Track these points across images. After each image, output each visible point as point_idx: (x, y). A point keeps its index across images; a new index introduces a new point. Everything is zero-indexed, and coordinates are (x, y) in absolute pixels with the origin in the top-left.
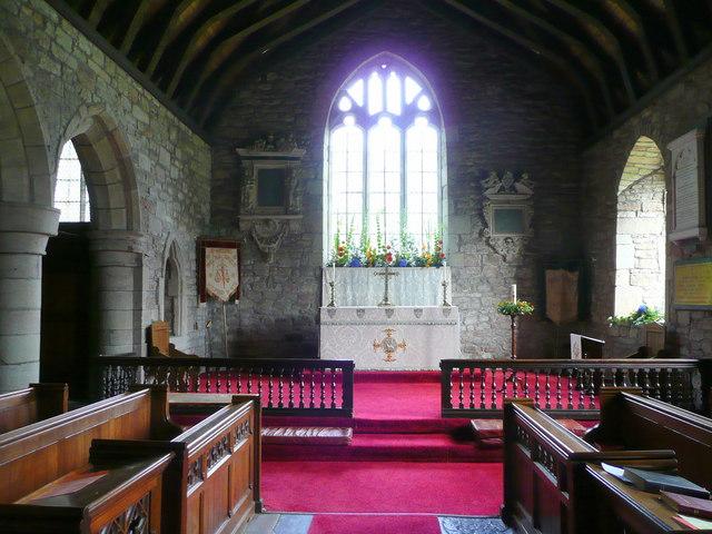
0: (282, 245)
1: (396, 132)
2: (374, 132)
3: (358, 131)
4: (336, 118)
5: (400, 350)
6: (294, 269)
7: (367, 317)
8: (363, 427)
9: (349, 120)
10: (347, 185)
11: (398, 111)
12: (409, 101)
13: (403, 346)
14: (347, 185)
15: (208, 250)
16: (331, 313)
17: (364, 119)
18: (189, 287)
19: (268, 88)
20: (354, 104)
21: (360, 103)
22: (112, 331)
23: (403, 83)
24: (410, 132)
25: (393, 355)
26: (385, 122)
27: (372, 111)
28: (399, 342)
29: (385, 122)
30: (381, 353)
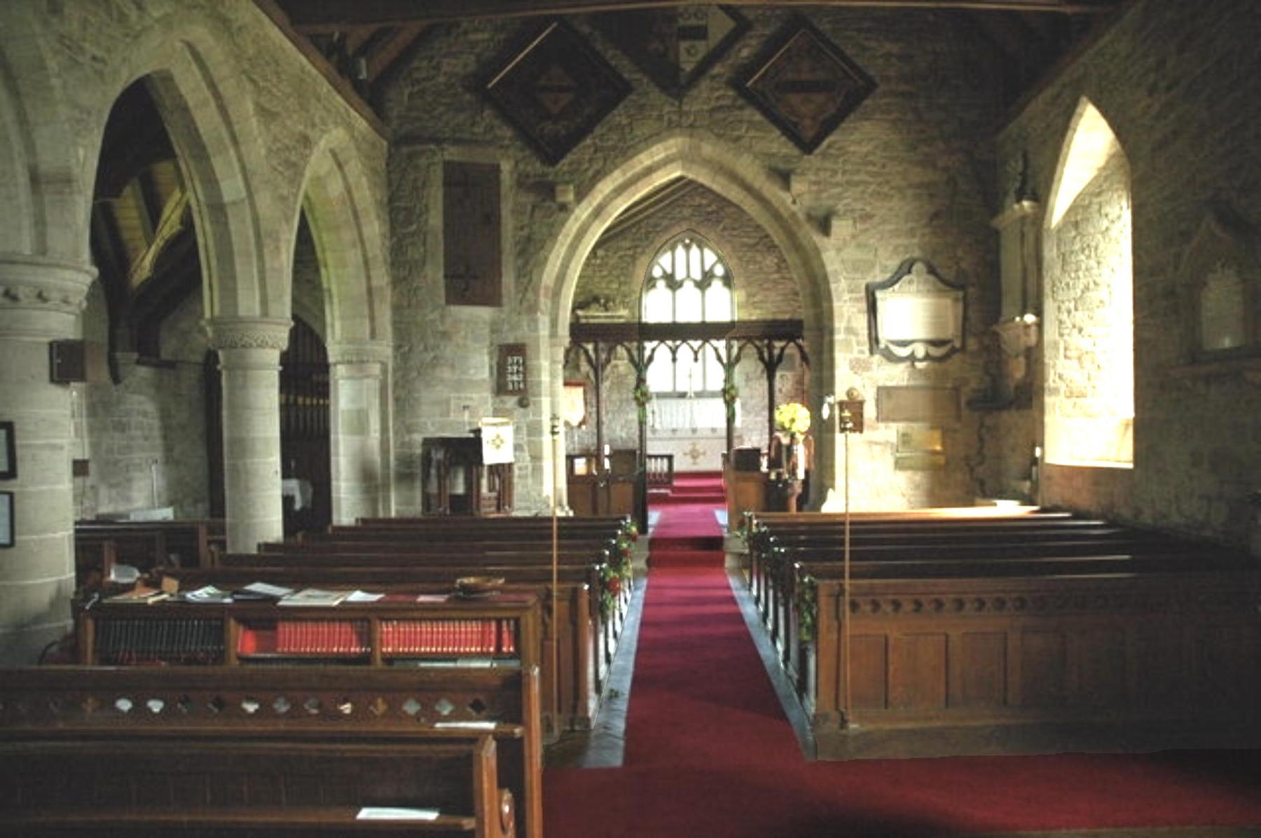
0: (613, 383)
1: (698, 292)
2: (679, 292)
3: (669, 292)
4: (650, 282)
5: (701, 457)
6: (621, 401)
7: (678, 434)
8: (674, 489)
9: (661, 284)
10: (847, 505)
11: (698, 276)
12: (707, 268)
13: (704, 453)
14: (847, 505)
17: (673, 283)
18: (347, 480)
19: (598, 261)
20: (664, 272)
21: (669, 271)
22: (1122, 166)
23: (688, 344)
24: (709, 291)
25: (698, 460)
26: (689, 285)
27: (679, 276)
28: (701, 451)
29: (689, 285)
30: (689, 459)
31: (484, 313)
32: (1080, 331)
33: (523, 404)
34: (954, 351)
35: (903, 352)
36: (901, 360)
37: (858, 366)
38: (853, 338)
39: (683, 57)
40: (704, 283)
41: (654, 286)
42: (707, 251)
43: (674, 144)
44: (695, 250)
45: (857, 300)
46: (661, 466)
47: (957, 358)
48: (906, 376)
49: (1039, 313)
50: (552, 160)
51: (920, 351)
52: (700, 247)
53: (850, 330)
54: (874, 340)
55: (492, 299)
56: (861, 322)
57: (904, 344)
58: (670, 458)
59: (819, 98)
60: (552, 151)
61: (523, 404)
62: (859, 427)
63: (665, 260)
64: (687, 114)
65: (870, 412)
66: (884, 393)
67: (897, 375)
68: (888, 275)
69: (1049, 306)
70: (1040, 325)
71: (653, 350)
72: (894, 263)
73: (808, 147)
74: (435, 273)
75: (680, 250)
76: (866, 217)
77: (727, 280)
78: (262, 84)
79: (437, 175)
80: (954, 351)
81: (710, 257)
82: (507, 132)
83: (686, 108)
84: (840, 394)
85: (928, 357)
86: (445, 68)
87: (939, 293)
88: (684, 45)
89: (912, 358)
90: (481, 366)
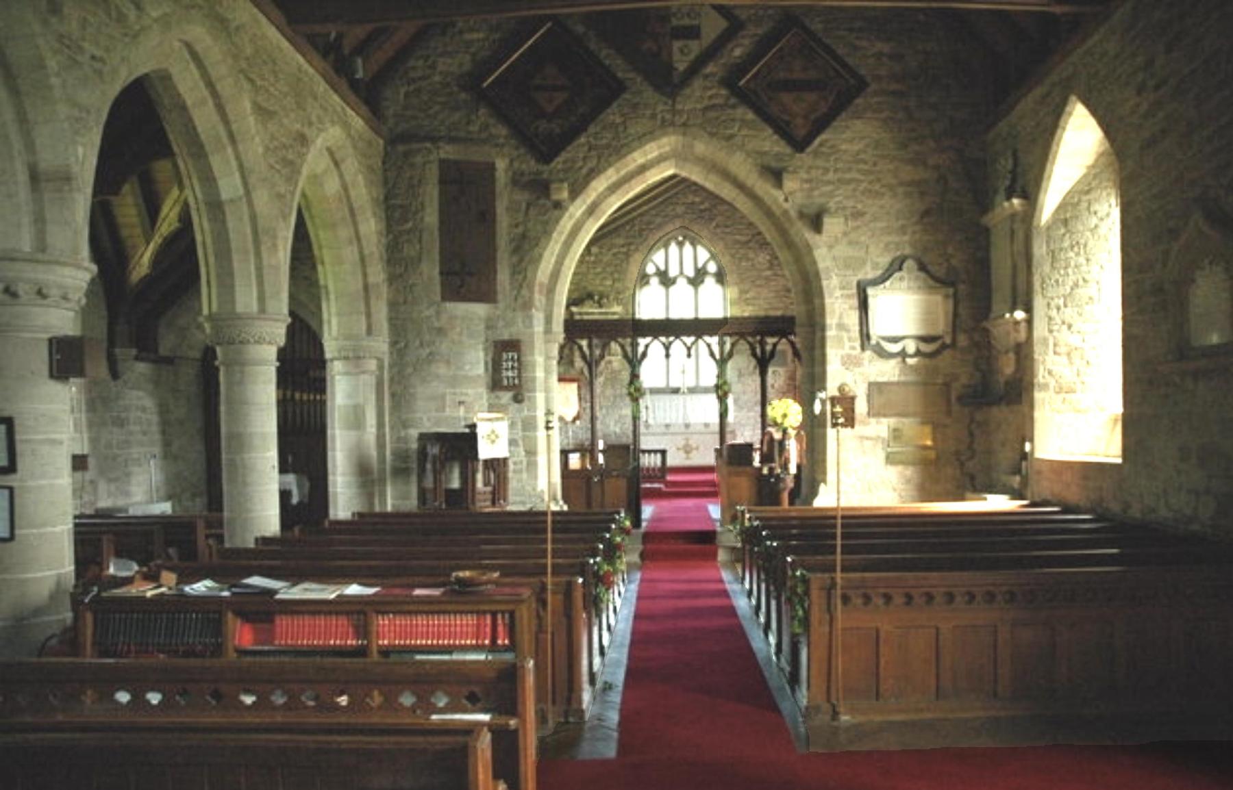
1: (691, 288)
2: (672, 289)
3: (662, 289)
4: (644, 279)
9: (655, 281)
15: (870, 291)
16: (647, 426)
17: (666, 280)
24: (702, 288)
26: (682, 282)
27: (673, 272)
29: (682, 282)
31: (479, 310)
32: (1070, 327)
33: (518, 399)
34: (944, 347)
35: (894, 348)
36: (892, 356)
37: (849, 362)
38: (845, 335)
39: (676, 56)
40: (697, 280)
41: (647, 283)
42: (700, 249)
43: (667, 143)
44: (688, 247)
45: (849, 296)
46: (655, 461)
47: (947, 354)
48: (897, 372)
49: (1029, 309)
50: (546, 158)
51: (911, 347)
52: (693, 244)
53: (841, 327)
54: (865, 336)
55: (486, 295)
56: (853, 318)
57: (895, 340)
58: (663, 452)
59: (811, 97)
60: (547, 149)
61: (518, 399)
62: (850, 422)
63: (658, 257)
64: (680, 112)
65: (861, 407)
66: (876, 388)
67: (888, 371)
68: (879, 272)
69: (1039, 303)
70: (1029, 322)
71: (647, 346)
72: (885, 260)
73: (800, 145)
74: (430, 270)
75: (673, 247)
76: (857, 215)
77: (720, 277)
78: (259, 83)
79: (433, 173)
80: (944, 347)
81: (703, 254)
82: (502, 131)
83: (679, 107)
84: (832, 389)
85: (918, 353)
86: (440, 67)
87: (930, 289)
88: (677, 45)
89: (903, 354)
90: (476, 362)
